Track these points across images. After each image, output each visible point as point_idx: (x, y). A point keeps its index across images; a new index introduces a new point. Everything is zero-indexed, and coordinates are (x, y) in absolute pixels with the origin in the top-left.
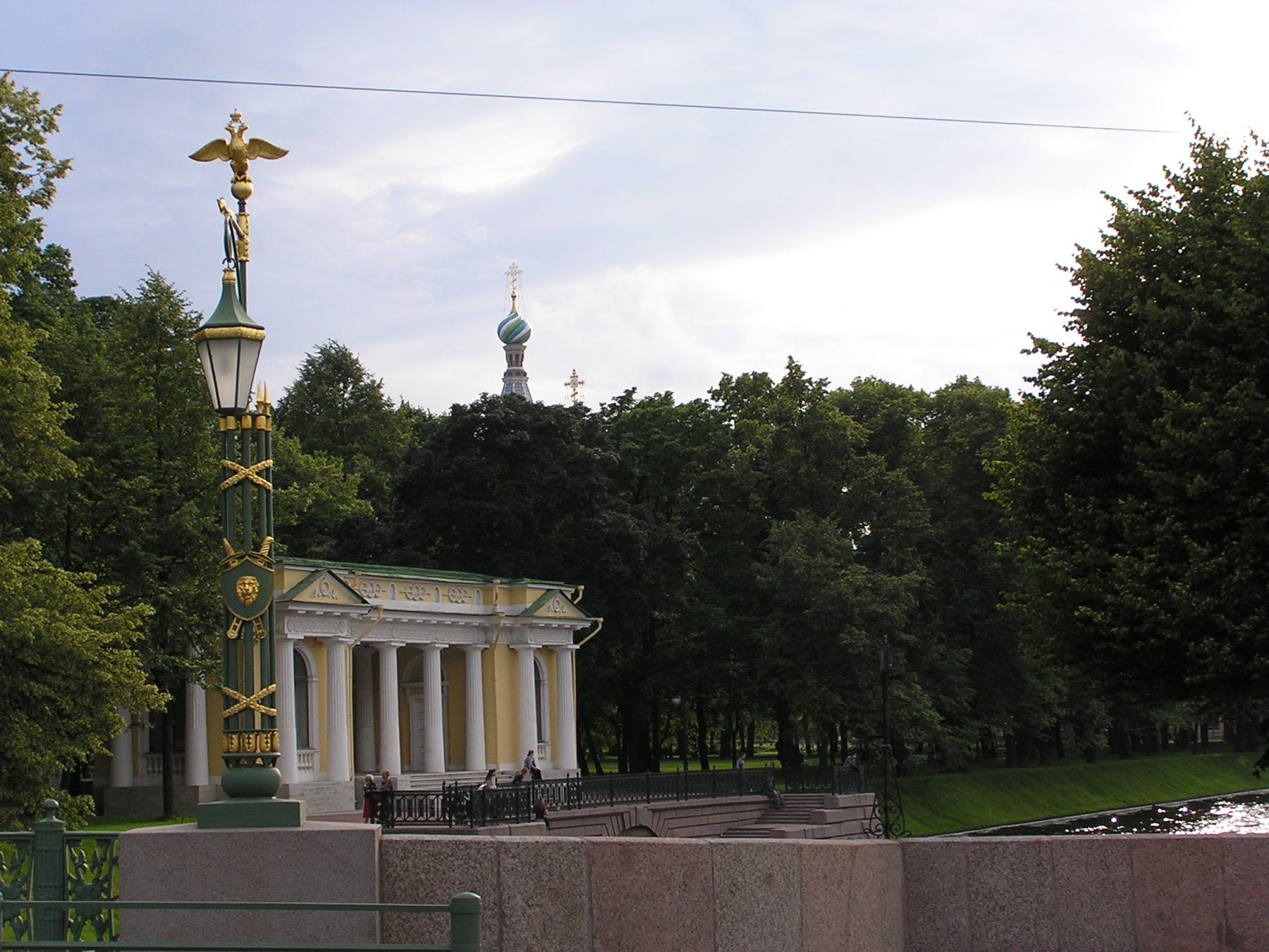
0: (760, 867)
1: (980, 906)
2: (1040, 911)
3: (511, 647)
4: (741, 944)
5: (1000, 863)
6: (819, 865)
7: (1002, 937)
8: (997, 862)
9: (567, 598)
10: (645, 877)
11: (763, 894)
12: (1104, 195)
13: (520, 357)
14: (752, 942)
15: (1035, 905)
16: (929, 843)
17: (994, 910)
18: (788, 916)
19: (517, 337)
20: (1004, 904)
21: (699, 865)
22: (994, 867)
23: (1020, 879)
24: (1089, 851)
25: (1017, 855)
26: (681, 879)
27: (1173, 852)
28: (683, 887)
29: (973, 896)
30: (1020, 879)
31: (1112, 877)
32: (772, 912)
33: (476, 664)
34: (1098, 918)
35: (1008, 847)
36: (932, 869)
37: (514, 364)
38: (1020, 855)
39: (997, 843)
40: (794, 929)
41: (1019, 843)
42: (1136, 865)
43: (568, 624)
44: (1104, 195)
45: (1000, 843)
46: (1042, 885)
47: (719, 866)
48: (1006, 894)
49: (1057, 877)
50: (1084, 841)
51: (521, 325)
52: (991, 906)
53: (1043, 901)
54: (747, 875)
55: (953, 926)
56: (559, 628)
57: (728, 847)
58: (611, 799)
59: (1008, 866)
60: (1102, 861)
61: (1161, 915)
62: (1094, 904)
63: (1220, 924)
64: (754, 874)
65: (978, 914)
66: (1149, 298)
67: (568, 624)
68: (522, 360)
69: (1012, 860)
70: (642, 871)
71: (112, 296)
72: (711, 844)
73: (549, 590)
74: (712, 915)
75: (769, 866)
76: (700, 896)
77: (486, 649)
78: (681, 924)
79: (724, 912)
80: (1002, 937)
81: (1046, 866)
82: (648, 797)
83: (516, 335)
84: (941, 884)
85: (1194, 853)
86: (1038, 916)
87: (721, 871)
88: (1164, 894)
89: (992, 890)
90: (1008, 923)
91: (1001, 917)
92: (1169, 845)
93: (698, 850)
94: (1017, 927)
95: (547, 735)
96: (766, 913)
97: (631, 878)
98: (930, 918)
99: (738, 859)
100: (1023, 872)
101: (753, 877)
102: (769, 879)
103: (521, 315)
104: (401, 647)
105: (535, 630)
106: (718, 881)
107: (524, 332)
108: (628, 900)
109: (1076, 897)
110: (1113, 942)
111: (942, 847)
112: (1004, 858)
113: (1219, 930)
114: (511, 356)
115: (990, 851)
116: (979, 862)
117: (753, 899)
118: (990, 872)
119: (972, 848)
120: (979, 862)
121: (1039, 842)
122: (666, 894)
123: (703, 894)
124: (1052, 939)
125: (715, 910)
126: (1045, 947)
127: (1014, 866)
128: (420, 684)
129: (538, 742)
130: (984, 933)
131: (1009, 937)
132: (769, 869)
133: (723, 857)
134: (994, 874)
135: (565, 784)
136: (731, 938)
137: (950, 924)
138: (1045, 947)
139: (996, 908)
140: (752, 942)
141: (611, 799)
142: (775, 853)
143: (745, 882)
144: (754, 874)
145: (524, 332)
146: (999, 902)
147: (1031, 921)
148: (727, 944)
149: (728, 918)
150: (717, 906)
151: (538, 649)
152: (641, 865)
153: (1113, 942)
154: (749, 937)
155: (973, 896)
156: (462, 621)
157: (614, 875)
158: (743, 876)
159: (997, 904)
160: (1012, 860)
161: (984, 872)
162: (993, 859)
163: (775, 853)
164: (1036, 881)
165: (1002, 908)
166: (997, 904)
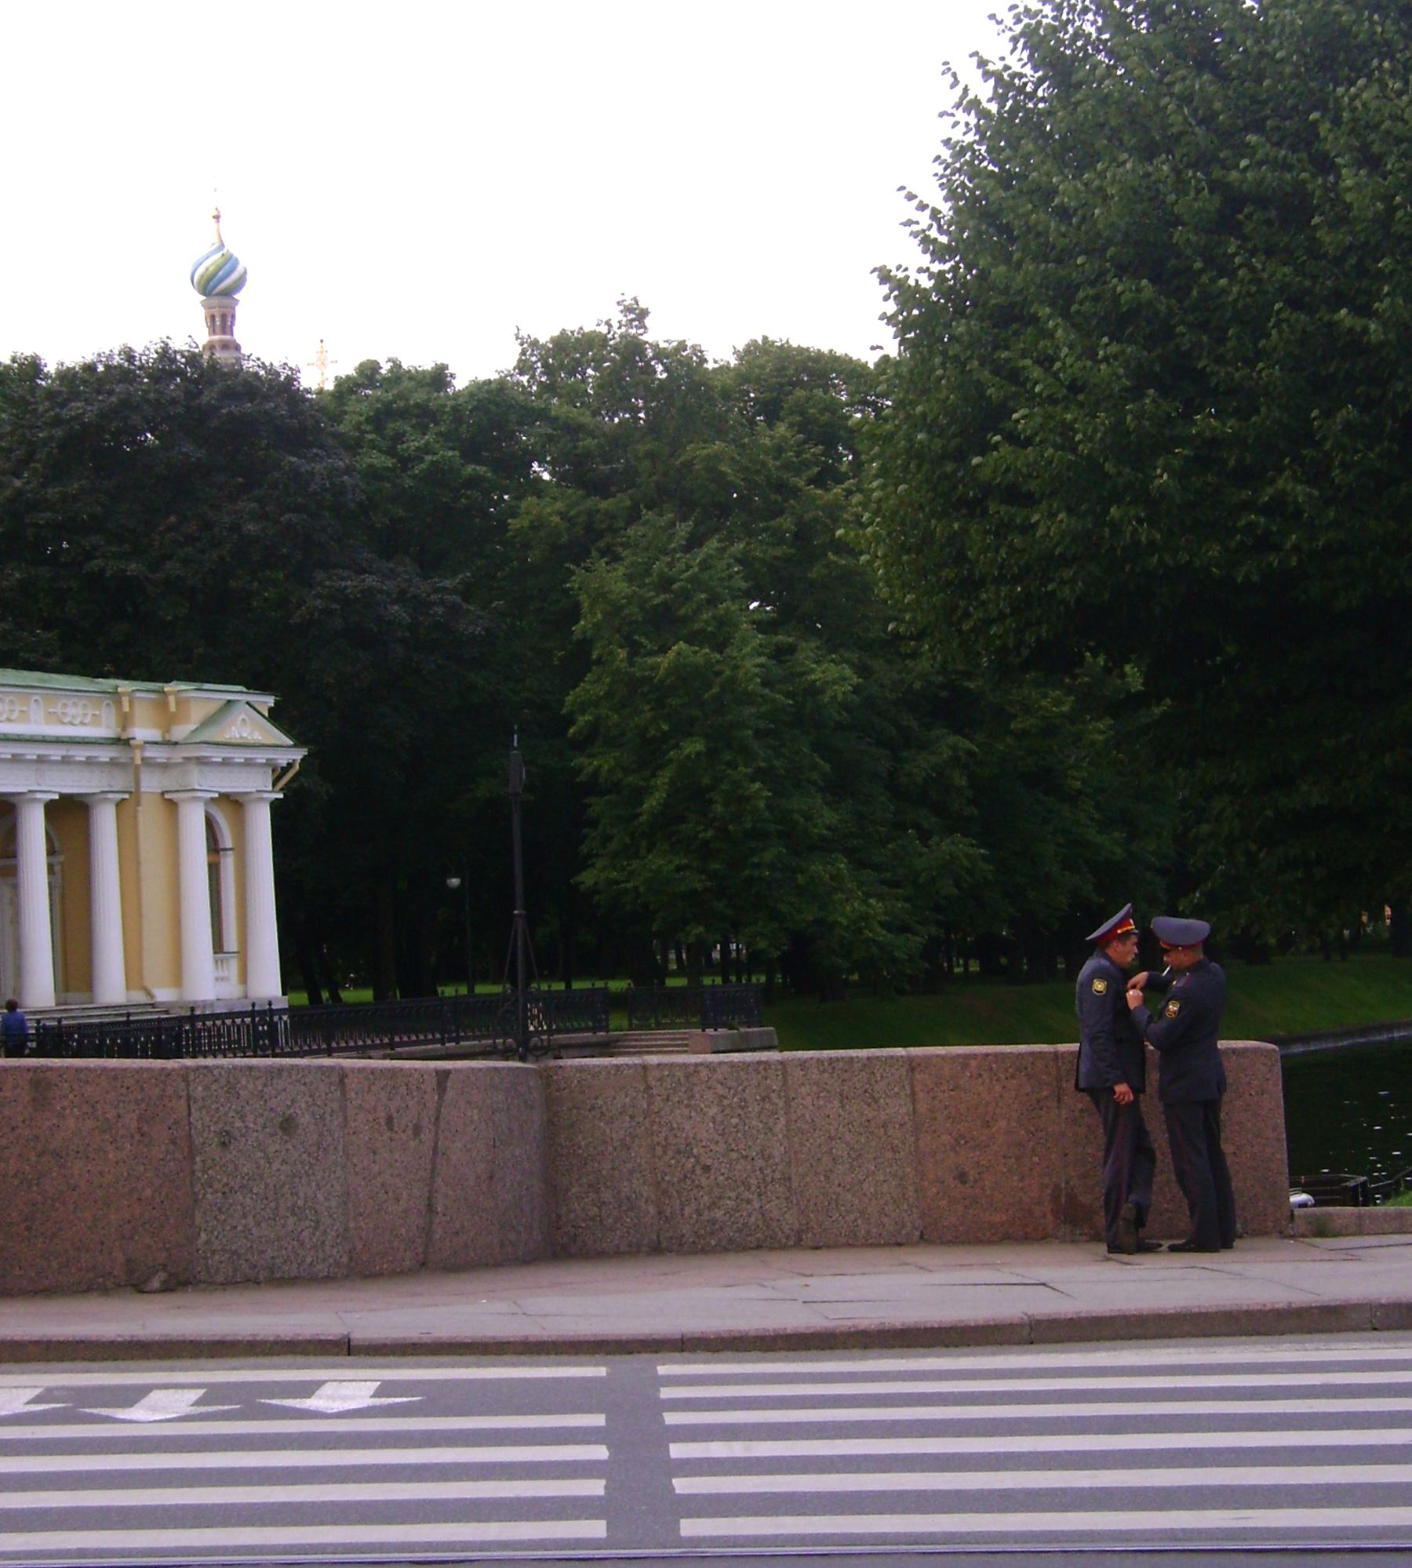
0: (273, 1103)
1: (670, 1166)
2: (768, 1171)
3: (167, 796)
4: (240, 1228)
5: (702, 1097)
6: (378, 1100)
7: (706, 1216)
8: (697, 1095)
9: (263, 716)
10: (71, 1122)
11: (277, 1147)
12: (975, 59)
13: (229, 319)
14: (258, 1224)
15: (760, 1163)
16: (588, 1066)
17: (693, 1172)
18: (322, 1183)
19: (223, 286)
20: (709, 1162)
21: (166, 1101)
22: (693, 1102)
23: (734, 1121)
24: (846, 1076)
25: (730, 1083)
26: (134, 1125)
27: (980, 1075)
28: (137, 1137)
29: (659, 1150)
30: (734, 1121)
31: (883, 1116)
32: (294, 1176)
33: (106, 825)
34: (861, 1182)
35: (715, 1070)
36: (593, 1108)
37: (218, 330)
38: (734, 1084)
39: (696, 1065)
40: (334, 1204)
41: (732, 1065)
42: (921, 1095)
43: (261, 757)
44: (975, 59)
45: (701, 1064)
46: (771, 1130)
47: (201, 1103)
48: (713, 1147)
49: (794, 1117)
50: (838, 1060)
51: (229, 263)
52: (689, 1166)
53: (771, 1156)
54: (250, 1118)
55: (628, 1198)
56: (249, 763)
57: (216, 1072)
58: (329, 1044)
59: (716, 1101)
60: (866, 1091)
61: (962, 1177)
62: (854, 1159)
63: (1057, 1187)
64: (262, 1115)
65: (667, 1178)
66: (1171, 237)
67: (261, 757)
68: (233, 324)
69: (721, 1090)
70: (68, 1111)
71: (598, 329)
72: (187, 1068)
73: (229, 701)
74: (188, 1182)
75: (289, 1103)
76: (167, 1152)
77: (123, 800)
78: (136, 1196)
79: (210, 1178)
80: (706, 1216)
81: (776, 1101)
82: (392, 1039)
83: (221, 281)
84: (608, 1131)
85: (1013, 1077)
86: (764, 1180)
87: (204, 1112)
88: (966, 1142)
89: (690, 1140)
90: (716, 1192)
91: (704, 1182)
92: (973, 1063)
93: (163, 1078)
94: (730, 1198)
95: (231, 942)
96: (282, 1177)
97: (48, 1123)
98: (590, 1186)
99: (232, 1089)
100: (740, 1111)
101: (260, 1121)
102: (288, 1125)
103: (231, 247)
104: (52, 801)
105: (206, 769)
106: (199, 1126)
107: (235, 276)
108: (43, 1159)
109: (825, 1149)
110: (885, 1220)
111: (609, 1073)
112: (710, 1088)
113: (1055, 1198)
114: (213, 317)
115: (687, 1077)
116: (668, 1096)
117: (259, 1154)
118: (686, 1112)
119: (657, 1074)
120: (668, 1096)
121: (766, 1064)
122: (110, 1148)
123: (172, 1147)
124: (787, 1216)
125: (193, 1172)
126: (777, 1229)
127: (726, 1102)
128: (9, 862)
129: (215, 953)
130: (677, 1207)
131: (719, 1214)
132: (289, 1107)
133: (207, 1088)
134: (693, 1114)
135: (248, 1020)
136: (223, 1217)
137: (623, 1195)
138: (777, 1229)
139: (698, 1168)
140: (258, 1224)
141: (329, 1044)
142: (299, 1081)
143: (246, 1127)
144: (262, 1115)
145: (235, 276)
146: (702, 1159)
147: (753, 1189)
148: (214, 1228)
149: (217, 1186)
150: (198, 1166)
151: (212, 799)
152: (66, 1103)
153: (885, 1220)
154: (254, 1217)
155: (659, 1150)
156: (80, 754)
157: (21, 1119)
158: (243, 1118)
159: (698, 1162)
160: (721, 1090)
161: (677, 1112)
162: (692, 1090)
163: (299, 1081)
164: (761, 1126)
165: (707, 1169)
166: (698, 1162)
